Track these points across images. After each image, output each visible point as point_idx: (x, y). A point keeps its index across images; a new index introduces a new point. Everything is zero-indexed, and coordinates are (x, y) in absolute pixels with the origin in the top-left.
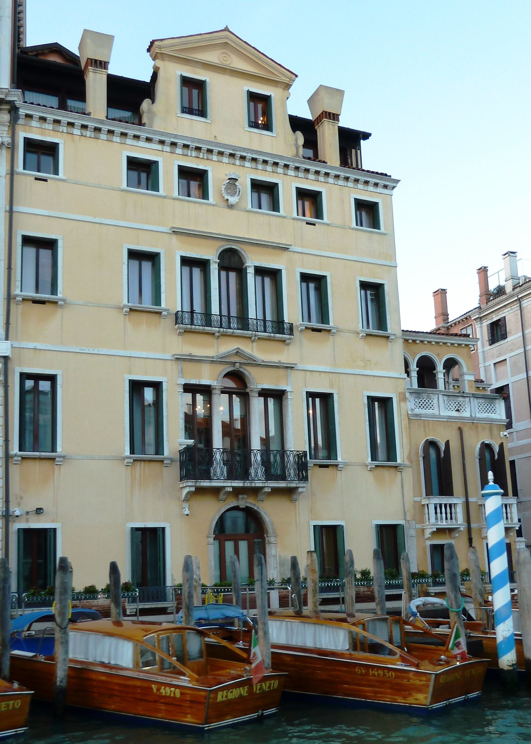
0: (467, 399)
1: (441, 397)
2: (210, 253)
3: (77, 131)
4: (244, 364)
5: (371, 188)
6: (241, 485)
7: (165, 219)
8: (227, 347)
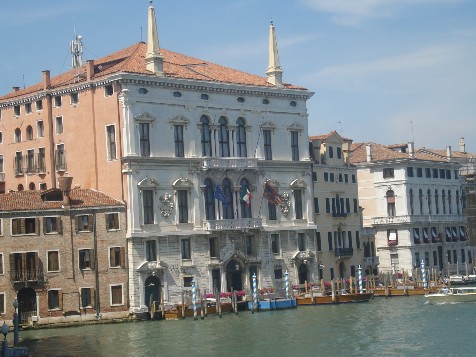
2: (335, 197)
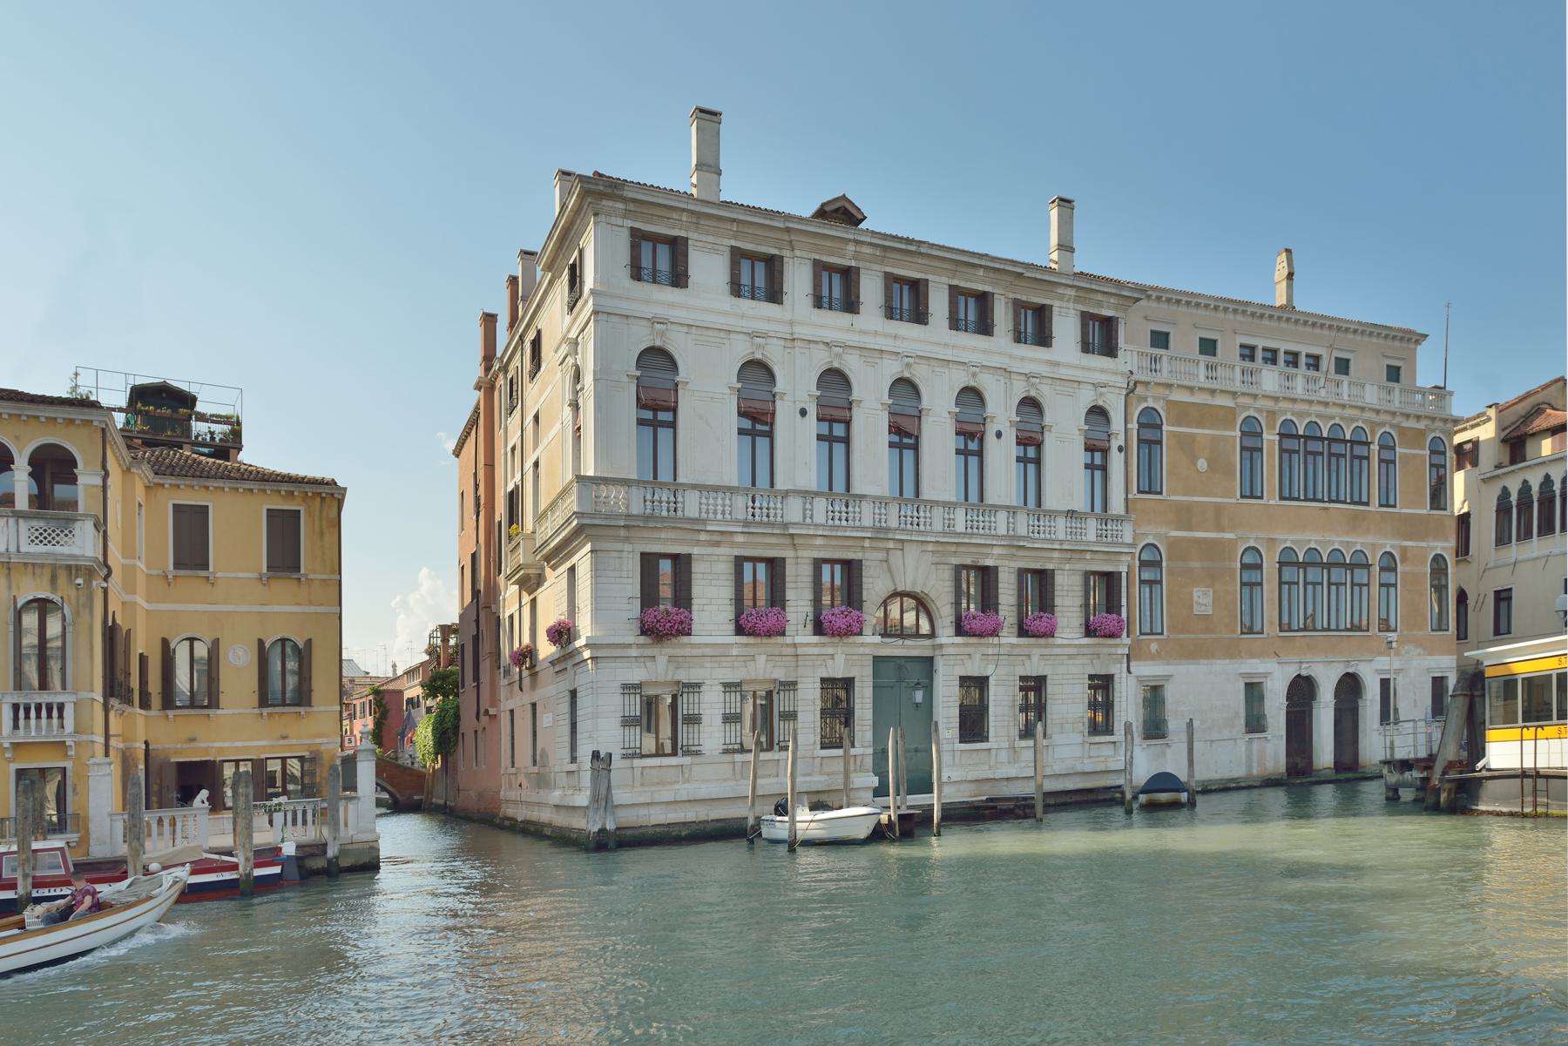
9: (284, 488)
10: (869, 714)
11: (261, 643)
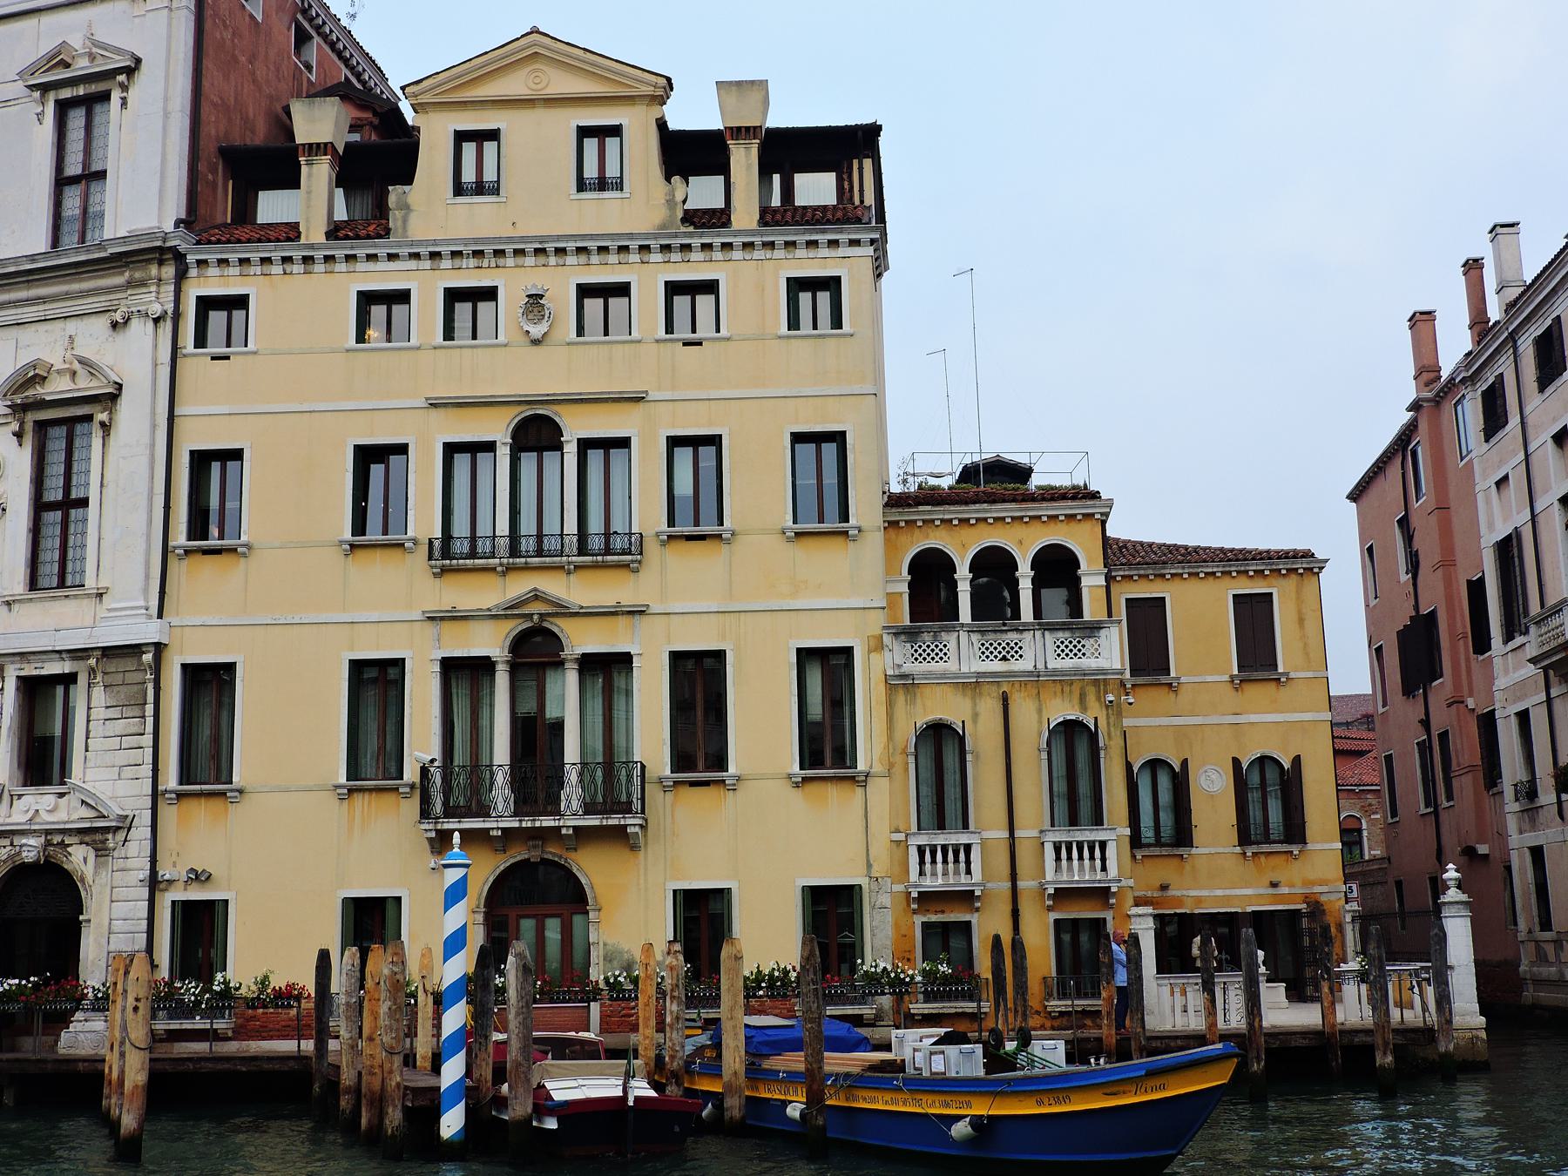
0: (1028, 636)
1: (963, 636)
3: (277, 269)
4: (549, 615)
5: (824, 252)
6: (597, 823)
7: (420, 389)
8: (518, 586)
9: (1253, 567)
10: (850, 1012)
11: (1236, 762)
